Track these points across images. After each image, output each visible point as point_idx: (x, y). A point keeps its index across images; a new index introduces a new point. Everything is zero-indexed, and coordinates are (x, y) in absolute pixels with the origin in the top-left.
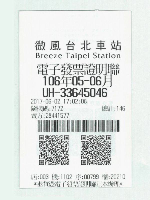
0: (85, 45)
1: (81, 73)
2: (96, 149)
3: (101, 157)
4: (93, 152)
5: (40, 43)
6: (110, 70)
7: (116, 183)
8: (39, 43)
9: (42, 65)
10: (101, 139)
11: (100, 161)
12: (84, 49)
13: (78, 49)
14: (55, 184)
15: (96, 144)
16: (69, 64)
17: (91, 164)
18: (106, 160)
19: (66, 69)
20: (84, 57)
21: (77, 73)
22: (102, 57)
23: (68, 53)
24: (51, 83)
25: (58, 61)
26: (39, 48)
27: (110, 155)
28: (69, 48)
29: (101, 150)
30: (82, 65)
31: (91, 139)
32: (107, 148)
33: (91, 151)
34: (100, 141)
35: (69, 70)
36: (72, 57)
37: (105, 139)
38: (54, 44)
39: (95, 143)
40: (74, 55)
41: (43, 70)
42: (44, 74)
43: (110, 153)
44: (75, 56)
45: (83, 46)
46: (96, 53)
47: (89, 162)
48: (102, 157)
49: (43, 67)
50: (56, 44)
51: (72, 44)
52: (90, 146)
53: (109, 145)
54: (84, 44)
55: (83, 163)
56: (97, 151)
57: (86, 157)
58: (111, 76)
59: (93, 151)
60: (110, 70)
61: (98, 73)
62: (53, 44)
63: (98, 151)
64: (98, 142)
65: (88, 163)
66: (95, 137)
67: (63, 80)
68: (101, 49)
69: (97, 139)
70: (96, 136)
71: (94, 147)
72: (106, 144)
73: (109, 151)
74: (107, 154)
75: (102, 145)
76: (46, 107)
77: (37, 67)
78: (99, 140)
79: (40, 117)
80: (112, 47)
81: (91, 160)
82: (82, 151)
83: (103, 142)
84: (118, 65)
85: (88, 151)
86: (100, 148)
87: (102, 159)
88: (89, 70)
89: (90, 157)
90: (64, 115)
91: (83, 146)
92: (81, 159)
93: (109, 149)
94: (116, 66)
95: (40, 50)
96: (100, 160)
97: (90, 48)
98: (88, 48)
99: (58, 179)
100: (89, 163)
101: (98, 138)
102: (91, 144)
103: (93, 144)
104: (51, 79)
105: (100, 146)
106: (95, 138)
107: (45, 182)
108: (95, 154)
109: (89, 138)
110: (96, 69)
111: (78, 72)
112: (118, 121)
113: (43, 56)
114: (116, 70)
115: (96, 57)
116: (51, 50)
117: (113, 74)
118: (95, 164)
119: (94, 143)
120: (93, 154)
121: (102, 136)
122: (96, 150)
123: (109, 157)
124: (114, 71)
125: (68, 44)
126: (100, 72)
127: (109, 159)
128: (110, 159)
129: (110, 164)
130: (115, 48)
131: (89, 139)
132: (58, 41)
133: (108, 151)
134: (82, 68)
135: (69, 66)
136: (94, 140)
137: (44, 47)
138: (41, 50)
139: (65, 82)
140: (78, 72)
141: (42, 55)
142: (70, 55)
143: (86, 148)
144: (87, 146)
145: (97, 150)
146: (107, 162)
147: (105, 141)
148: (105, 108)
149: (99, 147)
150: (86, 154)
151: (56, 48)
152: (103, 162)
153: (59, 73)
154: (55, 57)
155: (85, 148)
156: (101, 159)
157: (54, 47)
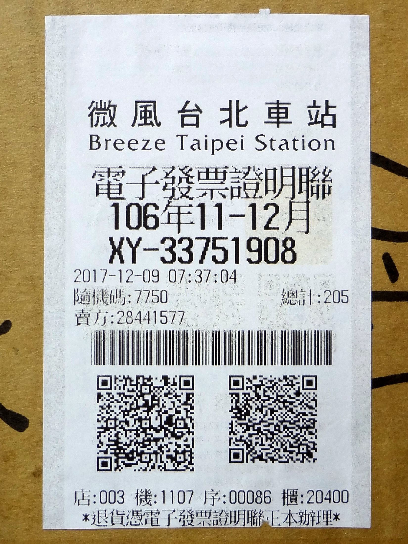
0: (233, 113)
1: (221, 194)
2: (273, 415)
3: (286, 441)
4: (265, 426)
5: (103, 107)
6: (304, 186)
7: (321, 514)
8: (99, 107)
9: (107, 170)
10: (288, 388)
11: (285, 450)
12: (228, 122)
13: (212, 125)
14: (144, 518)
15: (271, 400)
16: (186, 167)
17: (257, 460)
18: (301, 447)
19: (177, 181)
20: (229, 148)
21: (209, 192)
22: (282, 147)
23: (182, 136)
24: (134, 222)
25: (152, 157)
26: (98, 121)
27: (314, 434)
28: (187, 120)
29: (288, 419)
30: (222, 170)
31: (257, 386)
32: (304, 414)
33: (258, 421)
34: (284, 394)
35: (187, 185)
36: (195, 147)
37: (299, 387)
38: (143, 109)
39: (269, 398)
40: (199, 142)
41: (109, 184)
42: (112, 196)
43: (313, 427)
44: (202, 145)
45: (226, 115)
46: (264, 136)
47: (251, 453)
48: (290, 439)
49: (109, 176)
50: (148, 108)
51: (194, 110)
52: (254, 407)
53: (309, 404)
54: (230, 109)
55: (235, 457)
56: (275, 422)
57: (245, 441)
58: (308, 202)
59: (262, 421)
60: (304, 186)
61: (271, 194)
62: (139, 109)
63: (279, 424)
64: (278, 396)
65: (250, 458)
66: (271, 381)
67: (169, 214)
68: (278, 123)
69: (275, 387)
70: (272, 379)
71: (266, 411)
72: (301, 400)
73: (309, 421)
74: (305, 430)
75: (291, 403)
76: (119, 293)
77: (93, 177)
78: (282, 388)
79: (101, 320)
80: (311, 119)
81: (258, 448)
82: (231, 424)
83: (293, 396)
84: (328, 170)
85: (250, 421)
86: (284, 413)
87: (291, 446)
88: (245, 184)
89: (256, 438)
90: (170, 316)
91: (234, 407)
92: (230, 445)
93: (310, 416)
94: (323, 173)
95: (101, 126)
96: (284, 447)
97: (247, 122)
98: (241, 122)
99: (152, 502)
100: (252, 458)
101: (279, 383)
102: (257, 402)
103: (264, 401)
104: (134, 210)
105: (284, 408)
106: (269, 384)
107: (115, 512)
108: (268, 431)
109: (252, 385)
110: (264, 181)
111: (212, 191)
112: (328, 334)
113: (111, 144)
114: (324, 186)
115: (265, 146)
116: (133, 125)
117: (315, 196)
118: (269, 460)
119: (267, 398)
120: (265, 430)
121: (291, 376)
122: (273, 419)
123: (312, 438)
124: (318, 186)
125: (183, 110)
126: (275, 191)
127: (309, 445)
128: (314, 444)
129: (314, 460)
130: (319, 122)
131: (251, 388)
132: (154, 102)
133: (308, 423)
134: (225, 179)
135: (186, 174)
136: (266, 389)
137: (112, 119)
138: (105, 126)
139: (174, 218)
140: (212, 191)
141: (106, 141)
142: (188, 142)
143: (243, 413)
144: (247, 407)
145: (275, 418)
146: (305, 455)
147: (298, 393)
148: (290, 297)
149: (280, 411)
150: (244, 432)
151: (148, 121)
152: (294, 455)
153: (156, 194)
154: (147, 144)
155: (240, 413)
156: (286, 447)
157: (141, 118)
